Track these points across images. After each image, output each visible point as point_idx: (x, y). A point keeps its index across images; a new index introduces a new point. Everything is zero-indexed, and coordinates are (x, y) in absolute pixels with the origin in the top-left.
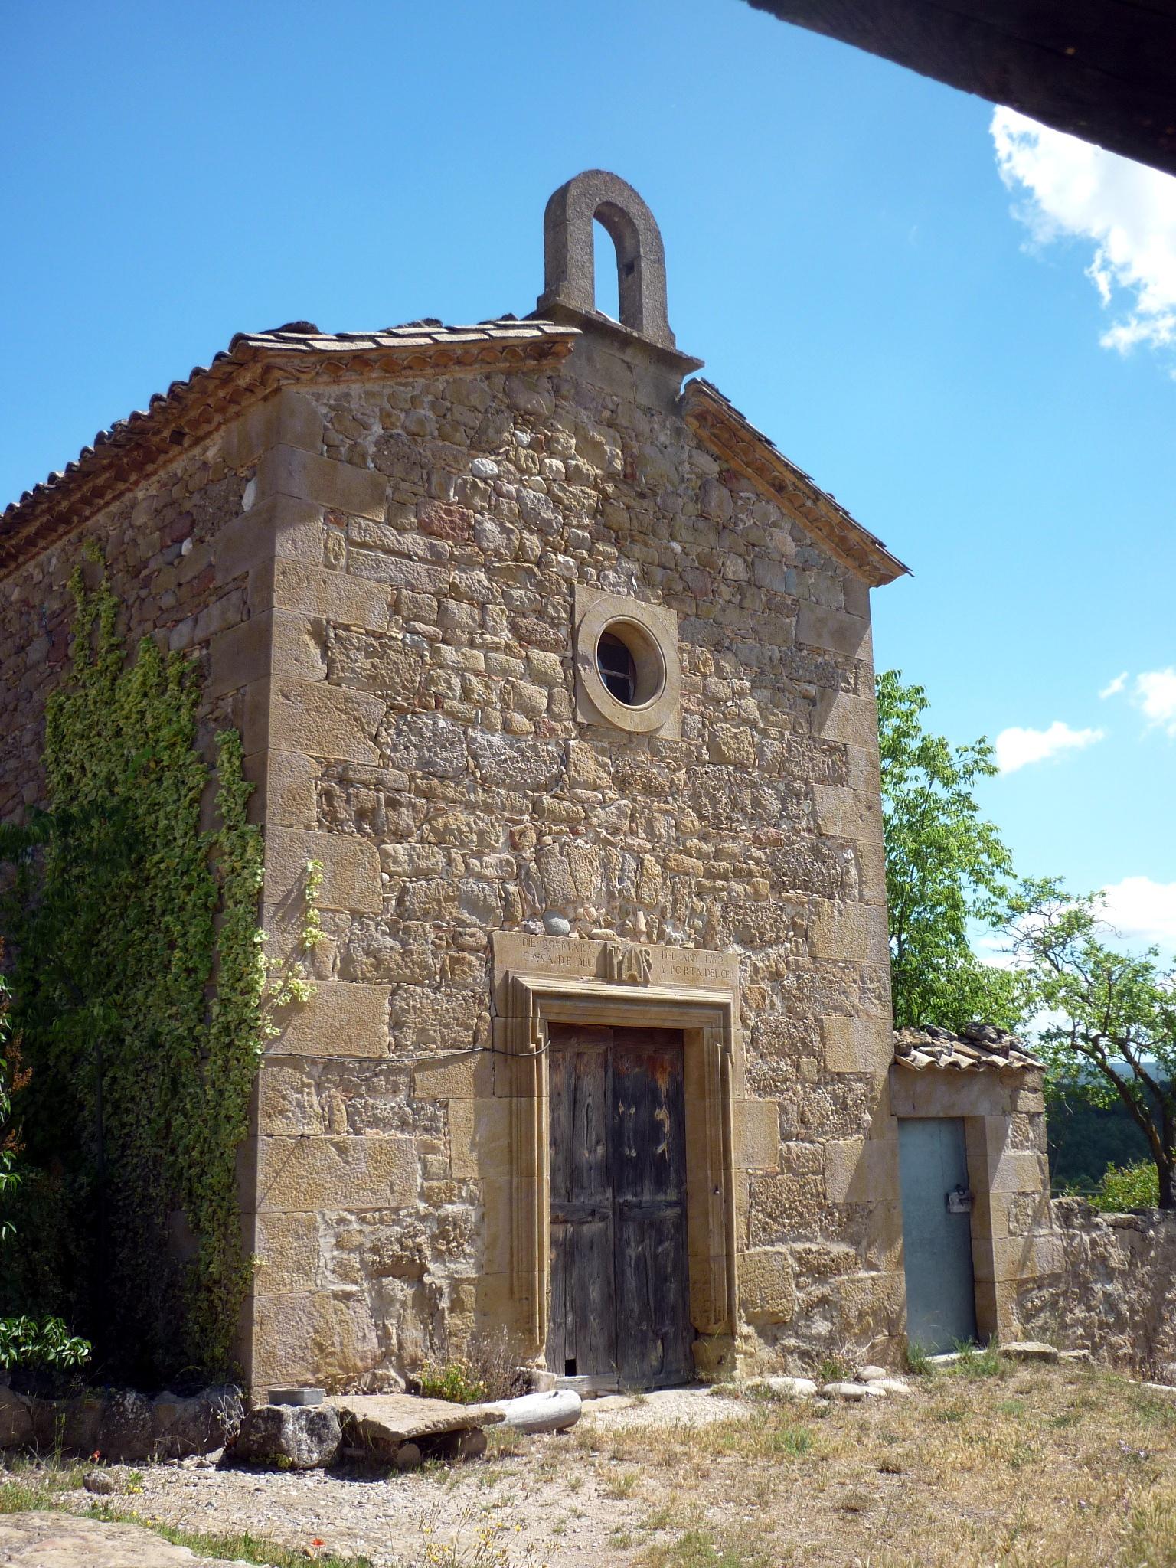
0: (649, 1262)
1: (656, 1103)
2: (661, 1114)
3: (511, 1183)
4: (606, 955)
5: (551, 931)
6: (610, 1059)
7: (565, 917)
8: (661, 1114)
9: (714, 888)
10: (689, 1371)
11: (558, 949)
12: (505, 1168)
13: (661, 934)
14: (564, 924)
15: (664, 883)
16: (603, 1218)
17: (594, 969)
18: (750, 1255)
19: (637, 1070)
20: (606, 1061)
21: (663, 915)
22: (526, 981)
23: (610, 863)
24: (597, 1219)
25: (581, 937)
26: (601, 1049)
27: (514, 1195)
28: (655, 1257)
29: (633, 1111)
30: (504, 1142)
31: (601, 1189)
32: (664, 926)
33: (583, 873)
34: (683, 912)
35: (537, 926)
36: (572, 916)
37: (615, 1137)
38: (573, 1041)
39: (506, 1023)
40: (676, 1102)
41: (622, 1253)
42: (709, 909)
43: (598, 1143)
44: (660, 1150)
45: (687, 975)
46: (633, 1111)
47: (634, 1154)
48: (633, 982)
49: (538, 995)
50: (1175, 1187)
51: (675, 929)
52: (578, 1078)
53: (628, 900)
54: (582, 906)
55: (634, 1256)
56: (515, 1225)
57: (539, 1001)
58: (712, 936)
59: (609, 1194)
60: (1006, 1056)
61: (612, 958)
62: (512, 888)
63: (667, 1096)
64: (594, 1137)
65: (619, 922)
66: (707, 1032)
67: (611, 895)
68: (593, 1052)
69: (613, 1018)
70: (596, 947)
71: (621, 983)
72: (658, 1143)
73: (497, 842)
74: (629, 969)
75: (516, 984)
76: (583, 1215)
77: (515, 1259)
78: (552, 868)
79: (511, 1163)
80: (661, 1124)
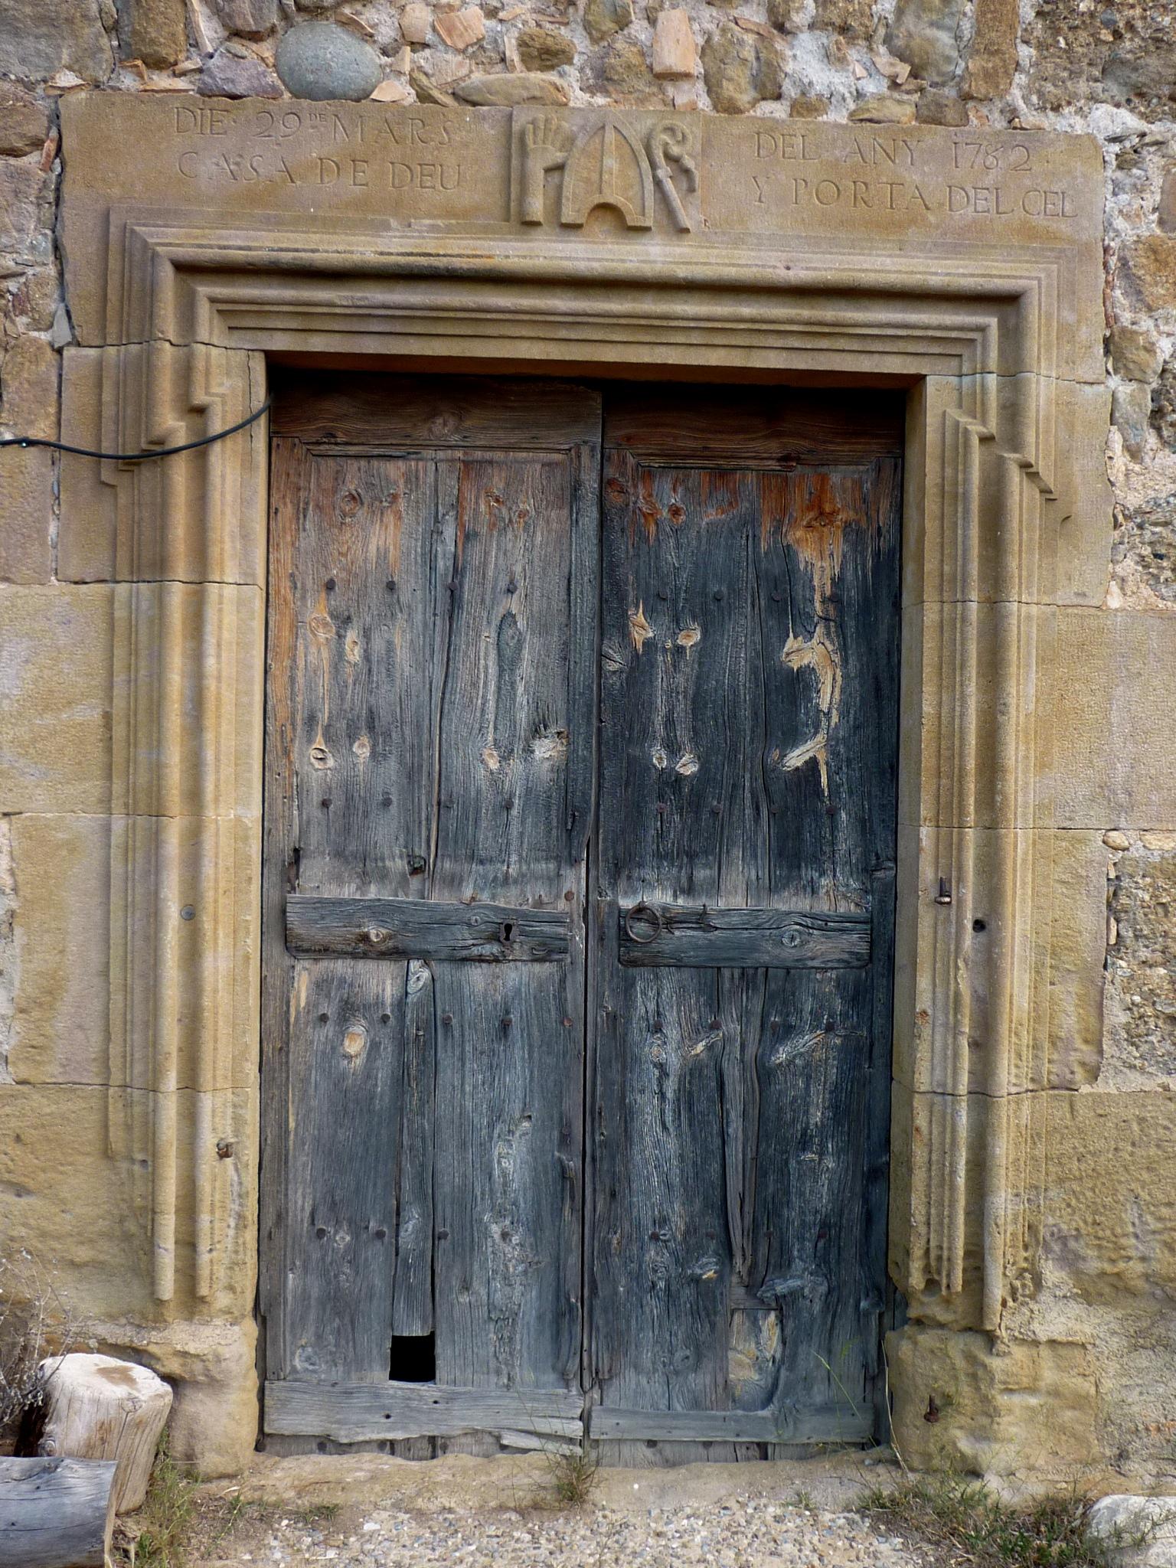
0: (735, 1088)
1: (783, 604)
2: (809, 652)
3: (107, 830)
8: (809, 652)
10: (974, 929)
12: (93, 787)
16: (548, 950)
18: (1098, 1099)
19: (711, 515)
24: (518, 951)
27: (117, 868)
28: (764, 1074)
29: (690, 638)
30: (89, 714)
31: (547, 867)
37: (607, 715)
39: (100, 364)
40: (875, 616)
41: (624, 1057)
43: (537, 730)
44: (796, 759)
46: (690, 638)
47: (688, 766)
55: (674, 1062)
56: (116, 953)
59: (575, 880)
63: (835, 599)
64: (523, 717)
68: (525, 530)
72: (793, 737)
76: (463, 937)
77: (115, 1050)
79: (109, 777)
80: (801, 683)
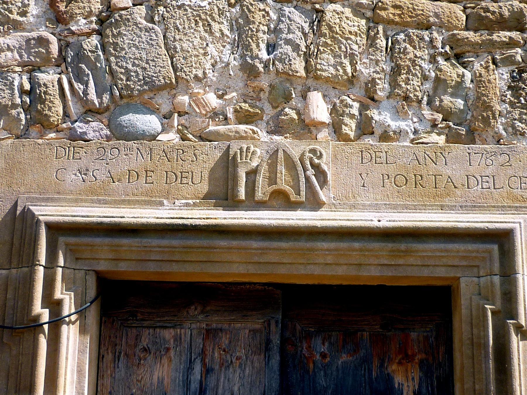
4: (228, 165)
5: (121, 134)
6: (276, 340)
7: (153, 111)
9: (492, 43)
11: (129, 158)
13: (365, 128)
14: (149, 122)
15: (372, 41)
17: (204, 188)
19: (344, 358)
20: (268, 342)
21: (370, 98)
22: (36, 210)
23: (248, 22)
25: (184, 138)
26: (256, 323)
32: (374, 114)
33: (191, 41)
34: (415, 86)
35: (94, 129)
36: (165, 108)
38: (193, 311)
42: (477, 80)
45: (417, 185)
48: (281, 200)
49: (56, 230)
50: (526, 334)
51: (399, 114)
52: (207, 371)
53: (289, 76)
54: (187, 90)
57: (62, 240)
58: (486, 121)
60: (346, 41)
61: (235, 165)
62: (48, 77)
65: (269, 111)
66: (466, 287)
67: (249, 71)
68: (245, 329)
69: (235, 266)
70: (212, 153)
71: (261, 205)
73: (23, 14)
74: (272, 180)
75: (27, 214)
78: (125, 41)
